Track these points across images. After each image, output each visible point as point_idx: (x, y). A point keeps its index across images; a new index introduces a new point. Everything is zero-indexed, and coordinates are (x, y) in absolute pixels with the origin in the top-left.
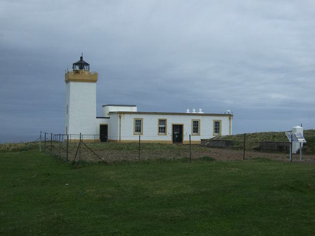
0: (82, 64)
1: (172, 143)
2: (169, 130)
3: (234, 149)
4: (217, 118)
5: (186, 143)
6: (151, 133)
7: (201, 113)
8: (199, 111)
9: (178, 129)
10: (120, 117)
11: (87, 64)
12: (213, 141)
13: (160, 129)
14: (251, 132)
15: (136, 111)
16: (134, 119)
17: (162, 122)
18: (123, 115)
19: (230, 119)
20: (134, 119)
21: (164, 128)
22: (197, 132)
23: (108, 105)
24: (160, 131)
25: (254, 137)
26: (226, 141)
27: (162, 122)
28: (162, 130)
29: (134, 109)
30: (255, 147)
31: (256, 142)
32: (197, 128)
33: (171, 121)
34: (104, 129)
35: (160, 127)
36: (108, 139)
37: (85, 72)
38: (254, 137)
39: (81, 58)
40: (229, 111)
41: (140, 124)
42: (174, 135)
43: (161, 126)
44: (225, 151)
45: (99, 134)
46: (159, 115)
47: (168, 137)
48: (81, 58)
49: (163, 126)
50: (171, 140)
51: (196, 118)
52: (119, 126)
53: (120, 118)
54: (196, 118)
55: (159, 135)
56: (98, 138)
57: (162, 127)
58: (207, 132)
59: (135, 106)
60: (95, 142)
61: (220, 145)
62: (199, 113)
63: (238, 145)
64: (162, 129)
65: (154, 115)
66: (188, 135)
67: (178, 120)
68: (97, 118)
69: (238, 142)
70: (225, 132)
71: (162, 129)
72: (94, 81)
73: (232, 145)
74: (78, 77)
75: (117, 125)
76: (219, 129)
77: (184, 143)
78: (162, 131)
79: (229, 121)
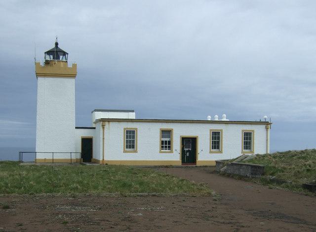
0: (56, 53)
1: (180, 164)
2: (177, 145)
3: (266, 182)
4: (248, 128)
5: (202, 165)
6: (149, 150)
7: (225, 120)
8: (222, 119)
9: (190, 143)
10: (103, 126)
11: (64, 54)
12: (233, 164)
13: (127, 143)
14: (300, 148)
15: (134, 118)
16: (125, 129)
17: (167, 133)
18: (107, 123)
19: (267, 129)
20: (125, 129)
21: (170, 142)
22: (250, 149)
23: (96, 110)
24: (162, 147)
25: (304, 158)
26: (252, 166)
27: (167, 133)
28: (166, 145)
29: (132, 116)
30: (305, 181)
31: (308, 170)
32: (218, 143)
33: (179, 132)
34: (87, 145)
35: (162, 142)
36: (95, 156)
37: (58, 66)
38: (304, 158)
39: (57, 44)
40: (266, 117)
41: (134, 137)
42: (183, 153)
43: (164, 139)
44: (248, 186)
45: (80, 150)
46: (161, 124)
47: (174, 156)
48: (57, 44)
49: (168, 139)
50: (179, 160)
51: (216, 127)
52: (101, 140)
53: (103, 128)
54: (216, 127)
55: (161, 152)
56: (79, 156)
57: (166, 142)
58: (232, 149)
59: (133, 111)
60: (71, 164)
61: (242, 172)
62: (223, 120)
63: (272, 174)
64: (166, 144)
65: (184, 124)
66: (205, 155)
67: (189, 131)
68: (76, 128)
69: (275, 167)
70: (260, 148)
71: (166, 144)
72: (73, 76)
73: (263, 174)
74: (49, 70)
75: (270, 144)
76: (250, 143)
77: (198, 164)
78: (166, 147)
79: (266, 132)
